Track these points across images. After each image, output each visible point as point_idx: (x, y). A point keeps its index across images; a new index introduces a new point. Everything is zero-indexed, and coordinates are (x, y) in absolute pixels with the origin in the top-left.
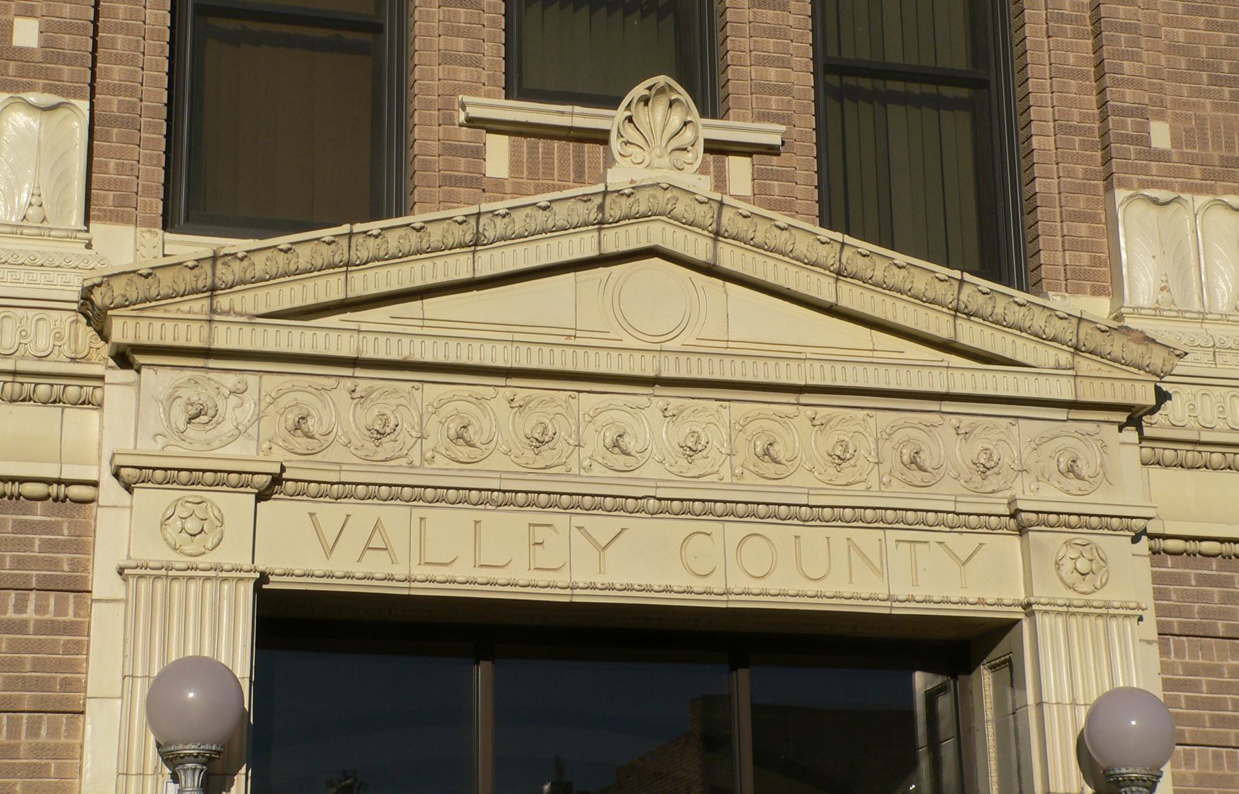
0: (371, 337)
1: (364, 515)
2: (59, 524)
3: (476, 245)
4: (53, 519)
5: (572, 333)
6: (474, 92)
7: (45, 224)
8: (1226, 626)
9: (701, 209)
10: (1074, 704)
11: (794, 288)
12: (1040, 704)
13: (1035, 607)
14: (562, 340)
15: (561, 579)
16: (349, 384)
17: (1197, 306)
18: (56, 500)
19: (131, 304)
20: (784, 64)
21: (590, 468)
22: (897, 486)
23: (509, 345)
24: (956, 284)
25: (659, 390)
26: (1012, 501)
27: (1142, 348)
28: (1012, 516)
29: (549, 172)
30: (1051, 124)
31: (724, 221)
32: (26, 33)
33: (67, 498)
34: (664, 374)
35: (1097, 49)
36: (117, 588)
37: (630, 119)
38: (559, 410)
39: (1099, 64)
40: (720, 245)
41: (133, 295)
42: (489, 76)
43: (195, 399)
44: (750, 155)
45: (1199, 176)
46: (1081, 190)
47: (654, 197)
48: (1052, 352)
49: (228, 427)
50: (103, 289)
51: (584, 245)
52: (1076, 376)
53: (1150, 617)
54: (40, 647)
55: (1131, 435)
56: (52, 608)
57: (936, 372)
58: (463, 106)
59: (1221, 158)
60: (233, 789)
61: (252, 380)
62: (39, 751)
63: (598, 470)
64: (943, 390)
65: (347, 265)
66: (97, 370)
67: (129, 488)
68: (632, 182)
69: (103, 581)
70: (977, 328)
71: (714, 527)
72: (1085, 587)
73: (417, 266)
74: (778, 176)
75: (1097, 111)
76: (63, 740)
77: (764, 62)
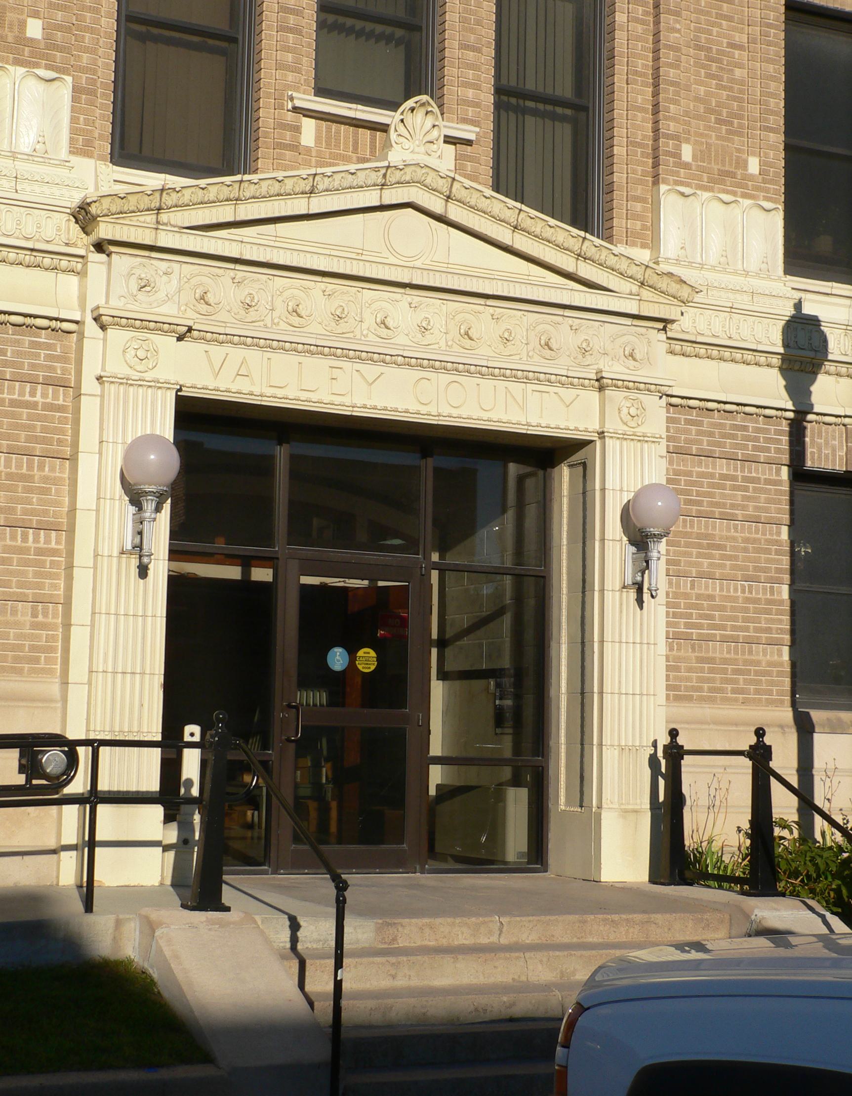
0: (248, 246)
1: (236, 354)
2: (54, 345)
3: (311, 193)
4: (51, 342)
5: (360, 251)
6: (297, 90)
7: (46, 155)
8: (697, 449)
9: (441, 182)
10: (621, 490)
11: (489, 234)
12: (603, 490)
13: (606, 434)
14: (354, 256)
15: (347, 400)
16: (232, 273)
17: (699, 260)
18: (53, 330)
19: (112, 214)
20: (477, 87)
21: (367, 336)
22: (537, 358)
23: (327, 257)
24: (581, 240)
25: (408, 291)
26: (599, 371)
27: (678, 286)
28: (597, 380)
29: (337, 146)
30: (625, 140)
31: (454, 190)
32: (34, 29)
33: (56, 327)
34: (414, 282)
35: (656, 94)
36: (96, 388)
37: (402, 121)
38: (351, 299)
39: (656, 105)
40: (449, 204)
41: (114, 209)
42: (305, 80)
43: (143, 276)
44: (455, 144)
45: (706, 180)
46: (641, 182)
47: (415, 172)
48: (629, 284)
49: (161, 295)
50: (97, 204)
51: (371, 198)
52: (640, 300)
53: (664, 442)
54: (44, 419)
55: (662, 336)
56: (50, 395)
57: (565, 292)
58: (292, 99)
59: (719, 170)
60: (163, 511)
61: (176, 266)
62: (45, 479)
63: (372, 337)
64: (568, 303)
65: (236, 200)
66: (82, 252)
67: (103, 327)
68: (404, 161)
69: (89, 385)
70: (588, 267)
71: (432, 375)
72: (633, 424)
73: (276, 203)
74: (471, 159)
75: (651, 134)
76: (58, 474)
77: (466, 85)
